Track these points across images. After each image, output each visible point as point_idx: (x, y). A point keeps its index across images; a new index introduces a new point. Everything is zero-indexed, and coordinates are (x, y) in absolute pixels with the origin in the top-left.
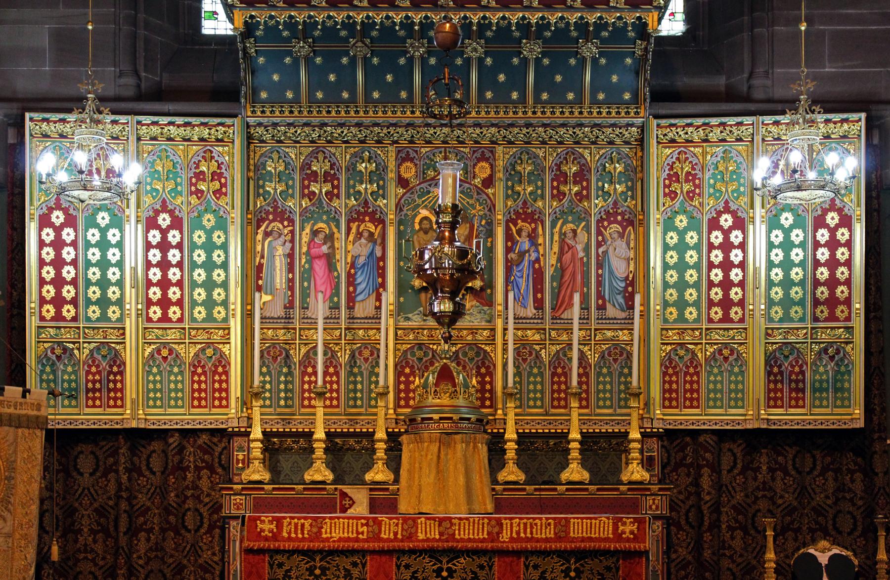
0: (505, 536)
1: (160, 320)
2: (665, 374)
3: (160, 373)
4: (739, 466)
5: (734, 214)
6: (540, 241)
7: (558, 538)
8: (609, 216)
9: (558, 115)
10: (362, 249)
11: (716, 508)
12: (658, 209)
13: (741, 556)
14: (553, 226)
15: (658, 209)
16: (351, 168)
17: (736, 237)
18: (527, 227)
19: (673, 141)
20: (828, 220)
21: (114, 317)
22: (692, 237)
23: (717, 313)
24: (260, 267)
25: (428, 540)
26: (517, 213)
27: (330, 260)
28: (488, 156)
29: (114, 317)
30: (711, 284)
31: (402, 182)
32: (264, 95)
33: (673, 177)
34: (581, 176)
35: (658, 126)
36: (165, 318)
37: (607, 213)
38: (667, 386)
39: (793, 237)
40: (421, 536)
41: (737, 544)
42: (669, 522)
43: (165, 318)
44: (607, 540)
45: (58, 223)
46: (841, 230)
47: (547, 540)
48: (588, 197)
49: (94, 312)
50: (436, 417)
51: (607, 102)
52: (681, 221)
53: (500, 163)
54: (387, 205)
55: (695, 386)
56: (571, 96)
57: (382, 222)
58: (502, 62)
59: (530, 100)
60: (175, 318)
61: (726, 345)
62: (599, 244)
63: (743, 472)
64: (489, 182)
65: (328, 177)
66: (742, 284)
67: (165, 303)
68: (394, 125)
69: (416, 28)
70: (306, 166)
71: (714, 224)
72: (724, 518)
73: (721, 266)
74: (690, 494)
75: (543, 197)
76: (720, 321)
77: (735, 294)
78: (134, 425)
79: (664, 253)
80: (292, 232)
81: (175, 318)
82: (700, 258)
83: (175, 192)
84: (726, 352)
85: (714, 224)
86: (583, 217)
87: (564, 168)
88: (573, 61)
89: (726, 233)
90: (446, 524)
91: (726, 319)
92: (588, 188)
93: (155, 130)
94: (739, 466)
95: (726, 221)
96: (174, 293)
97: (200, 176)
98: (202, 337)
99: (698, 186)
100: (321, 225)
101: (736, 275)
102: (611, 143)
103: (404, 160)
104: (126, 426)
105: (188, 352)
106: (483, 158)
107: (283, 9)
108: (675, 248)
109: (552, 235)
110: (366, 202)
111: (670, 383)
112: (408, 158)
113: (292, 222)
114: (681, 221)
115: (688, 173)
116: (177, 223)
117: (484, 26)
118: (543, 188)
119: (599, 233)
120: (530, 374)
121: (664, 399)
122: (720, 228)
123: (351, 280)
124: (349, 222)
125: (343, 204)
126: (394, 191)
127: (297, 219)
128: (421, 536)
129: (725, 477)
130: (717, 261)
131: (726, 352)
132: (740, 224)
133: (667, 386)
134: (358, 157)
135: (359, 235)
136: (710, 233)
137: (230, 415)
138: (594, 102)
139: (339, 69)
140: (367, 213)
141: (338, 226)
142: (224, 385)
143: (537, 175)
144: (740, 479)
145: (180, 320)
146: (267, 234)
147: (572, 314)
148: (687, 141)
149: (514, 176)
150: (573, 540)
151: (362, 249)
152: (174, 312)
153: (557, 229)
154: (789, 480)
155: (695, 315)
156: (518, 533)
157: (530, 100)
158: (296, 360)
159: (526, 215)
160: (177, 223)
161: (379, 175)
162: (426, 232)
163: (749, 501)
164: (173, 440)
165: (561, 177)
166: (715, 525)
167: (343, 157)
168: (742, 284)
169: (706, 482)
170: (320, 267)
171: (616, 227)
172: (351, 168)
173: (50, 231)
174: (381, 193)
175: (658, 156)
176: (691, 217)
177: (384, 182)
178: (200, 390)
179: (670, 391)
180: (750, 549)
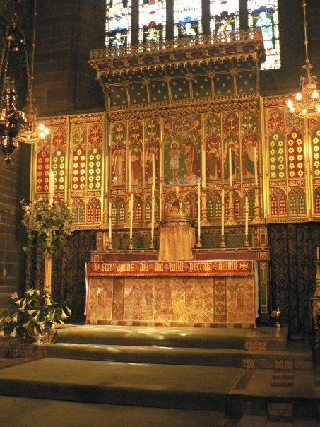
0: (191, 269)
1: (77, 189)
2: (271, 200)
3: (295, 199)
4: (305, 238)
5: (297, 132)
6: (220, 149)
7: (214, 271)
8: (247, 137)
9: (164, 105)
11: (296, 256)
12: (266, 133)
13: (307, 277)
14: (225, 142)
15: (266, 133)
17: (299, 142)
18: (215, 144)
19: (271, 105)
20: (293, 136)
21: (300, 175)
22: (280, 143)
23: (292, 174)
24: (113, 168)
25: (158, 272)
26: (210, 139)
28: (199, 118)
29: (300, 175)
30: (289, 162)
32: (115, 103)
33: (272, 120)
34: (236, 122)
35: (264, 99)
36: (79, 188)
37: (246, 136)
38: (273, 205)
39: (81, 158)
40: (156, 270)
41: (305, 272)
42: (270, 264)
43: (79, 188)
44: (234, 271)
45: (79, 154)
46: (298, 140)
47: (208, 272)
48: (238, 131)
49: (91, 186)
50: (177, 220)
51: (158, 100)
52: (276, 137)
53: (203, 120)
55: (284, 205)
56: (144, 100)
59: (236, 92)
60: (82, 188)
61: (297, 187)
62: (243, 149)
63: (307, 240)
64: (199, 128)
65: (138, 131)
66: (302, 161)
67: (79, 182)
68: (179, 107)
71: (290, 137)
72: (299, 261)
73: (293, 154)
74: (284, 251)
75: (220, 132)
76: (294, 177)
77: (300, 165)
78: (310, 220)
79: (313, 147)
80: (125, 153)
81: (82, 188)
82: (284, 152)
84: (297, 190)
85: (290, 137)
86: (236, 138)
87: (229, 120)
88: (228, 78)
89: (295, 140)
90: (166, 265)
91: (296, 176)
92: (238, 127)
93: (82, 119)
94: (305, 238)
95: (295, 135)
96: (82, 179)
98: (91, 195)
99: (283, 123)
100: (136, 149)
101: (300, 158)
102: (246, 108)
103: (167, 122)
104: (307, 221)
105: (86, 201)
106: (196, 119)
107: (192, 59)
108: (274, 148)
109: (224, 147)
110: (152, 140)
111: (274, 204)
113: (125, 149)
114: (276, 137)
115: (278, 118)
116: (84, 153)
118: (220, 128)
119: (243, 144)
120: (80, 209)
121: (271, 211)
122: (292, 139)
124: (146, 147)
125: (144, 141)
127: (127, 148)
128: (156, 270)
129: (299, 244)
130: (291, 152)
131: (297, 190)
132: (300, 136)
133: (273, 205)
135: (150, 152)
136: (288, 141)
137: (99, 224)
139: (161, 88)
141: (142, 150)
142: (303, 204)
143: (123, 132)
144: (306, 244)
145: (84, 189)
146: (116, 155)
147: (152, 181)
148: (276, 105)
149: (209, 124)
150: (220, 272)
152: (82, 186)
153: (226, 144)
154: (72, 250)
155: (283, 175)
156: (196, 269)
157: (236, 92)
158: (287, 194)
159: (214, 139)
160: (84, 153)
162: (175, 149)
163: (310, 253)
164: (92, 232)
165: (227, 123)
166: (296, 263)
168: (302, 161)
169: (291, 246)
171: (250, 142)
173: (292, 141)
174: (158, 135)
175: (264, 113)
176: (280, 135)
178: (91, 215)
179: (274, 207)
180: (311, 274)
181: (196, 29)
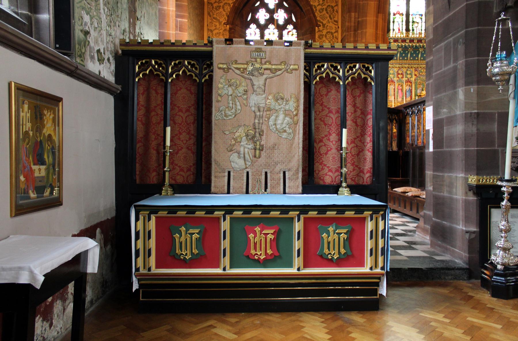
10: (408, 88)
16: (406, 72)
27: (402, 90)
31: (416, 75)
54: (413, 79)
57: (411, 83)
58: (415, 52)
65: (402, 74)
69: (144, 61)
70: (397, 72)
83: (394, 77)
97: (399, 74)
112: (416, 71)
117: (402, 46)
123: (406, 93)
125: (405, 79)
126: (414, 77)
134: (407, 70)
138: (400, 60)
139: (405, 54)
140: (408, 81)
151: (408, 88)
161: (411, 74)
167: (405, 70)
170: (400, 91)
172: (406, 72)
174: (412, 77)
177: (56, 46)
181: (421, 19)
